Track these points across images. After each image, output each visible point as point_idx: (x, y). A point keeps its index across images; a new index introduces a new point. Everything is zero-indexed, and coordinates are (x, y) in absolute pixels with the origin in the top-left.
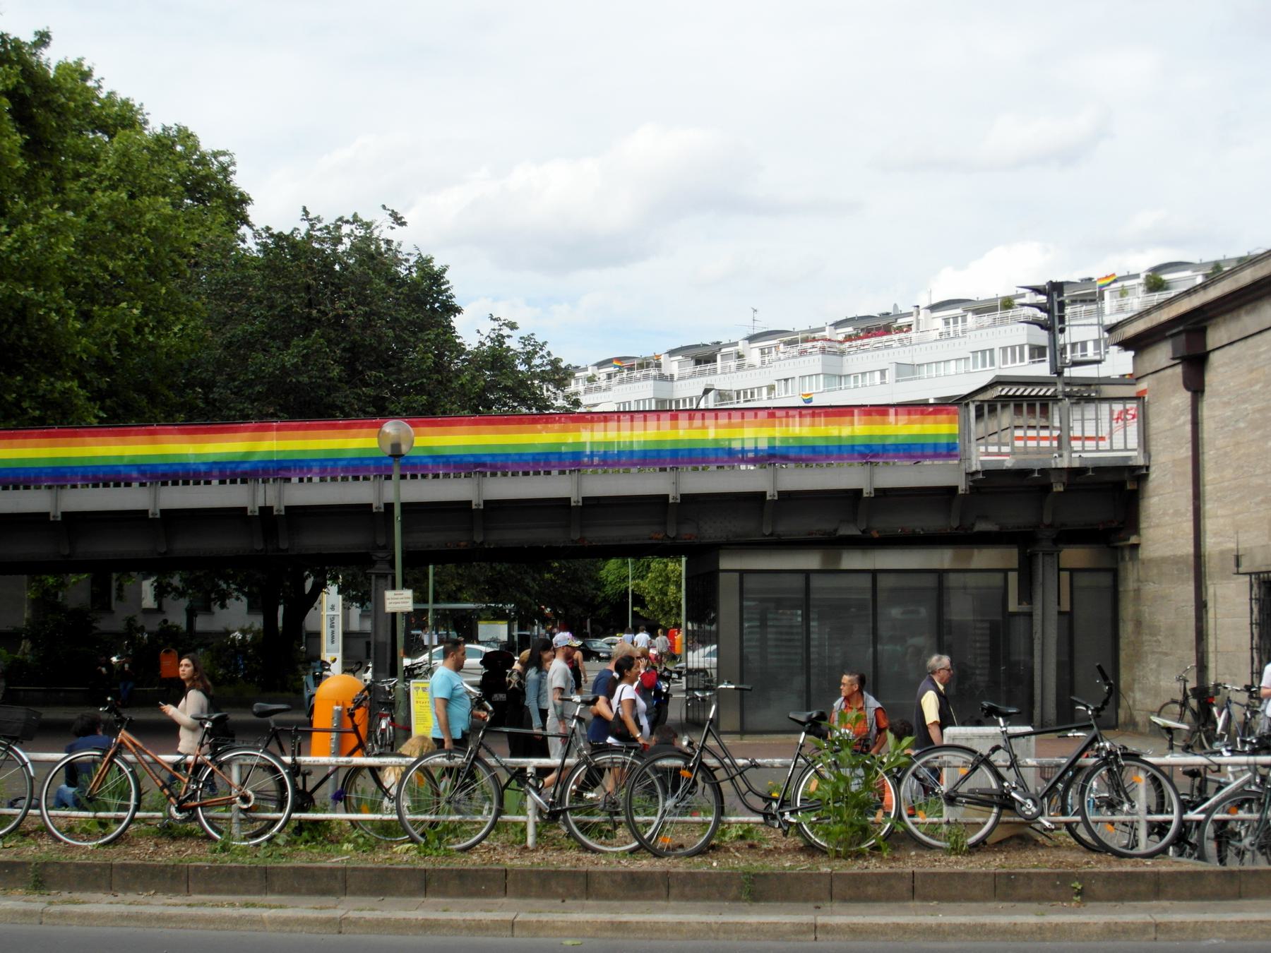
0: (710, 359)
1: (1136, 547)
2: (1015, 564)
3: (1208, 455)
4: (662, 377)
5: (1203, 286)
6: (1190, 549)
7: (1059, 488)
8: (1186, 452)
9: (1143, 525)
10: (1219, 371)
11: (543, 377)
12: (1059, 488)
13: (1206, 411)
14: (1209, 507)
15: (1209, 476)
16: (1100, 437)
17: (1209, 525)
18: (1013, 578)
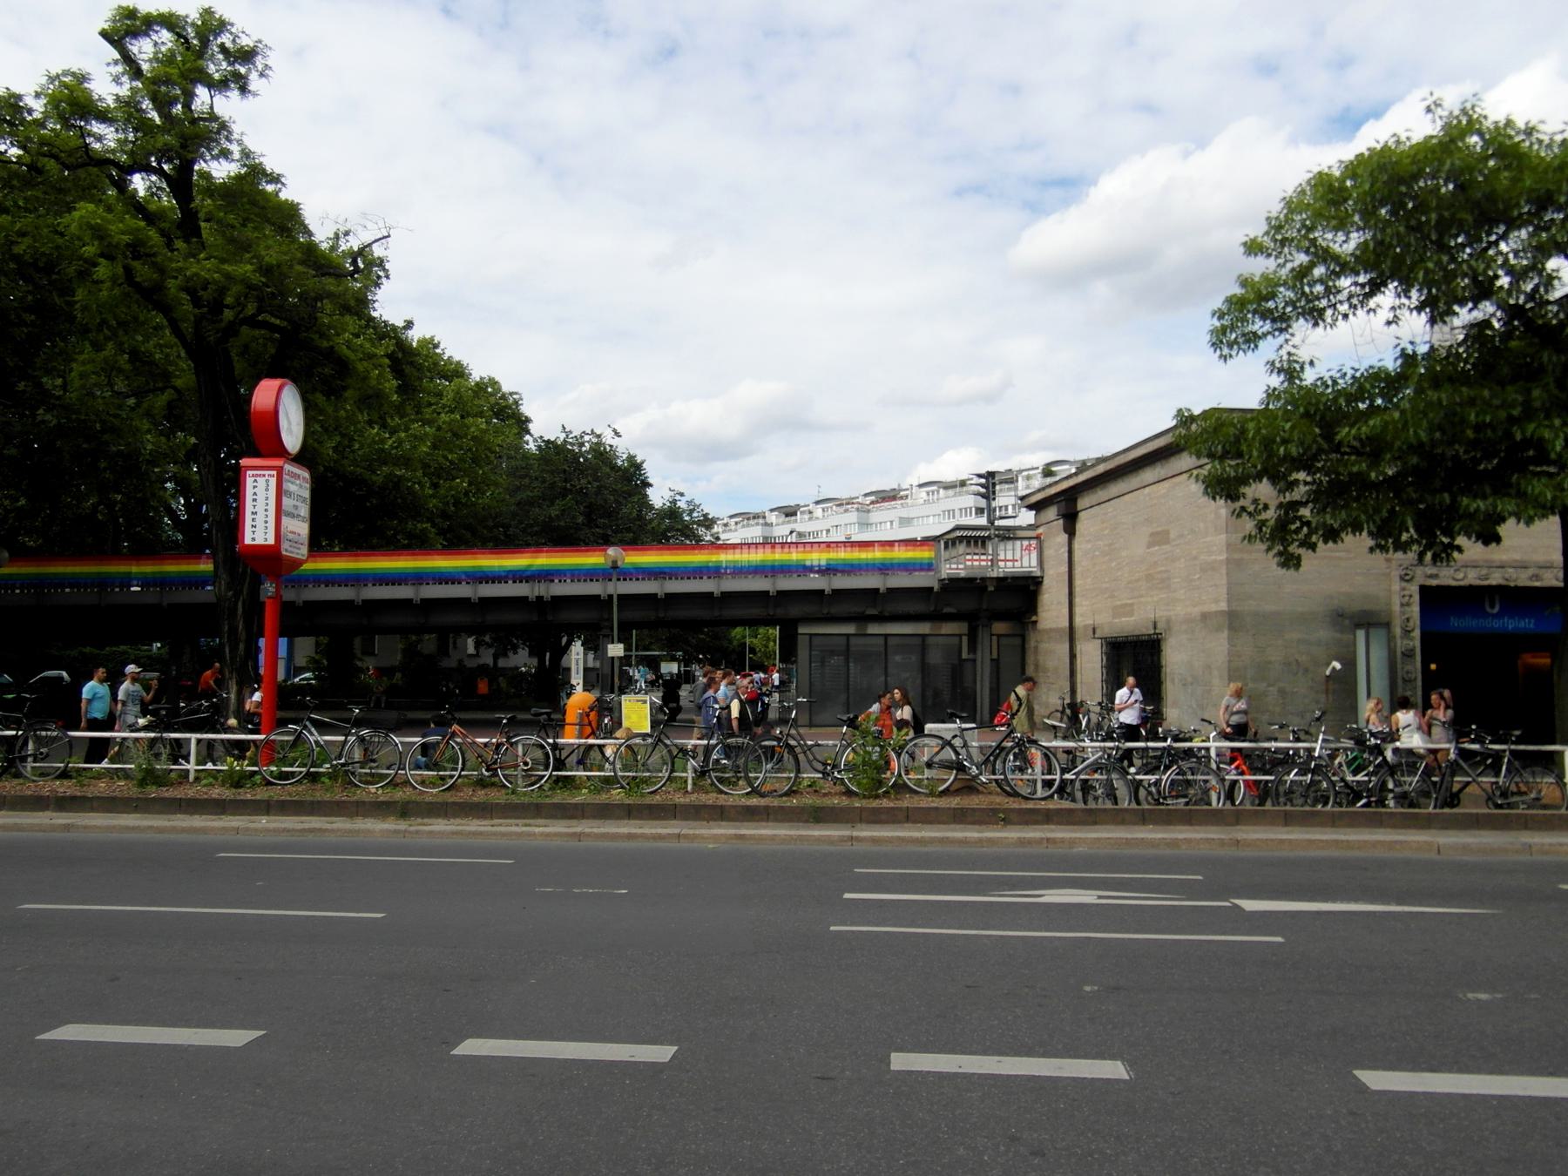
0: (794, 514)
1: (1035, 622)
2: (965, 631)
3: (1078, 570)
4: (766, 524)
5: (1076, 474)
6: (1067, 624)
7: (991, 588)
8: (1065, 568)
9: (1040, 610)
10: (1084, 523)
11: (699, 523)
12: (991, 588)
13: (1076, 546)
14: (1077, 600)
15: (1078, 582)
16: (1015, 560)
17: (1078, 610)
18: (965, 639)
